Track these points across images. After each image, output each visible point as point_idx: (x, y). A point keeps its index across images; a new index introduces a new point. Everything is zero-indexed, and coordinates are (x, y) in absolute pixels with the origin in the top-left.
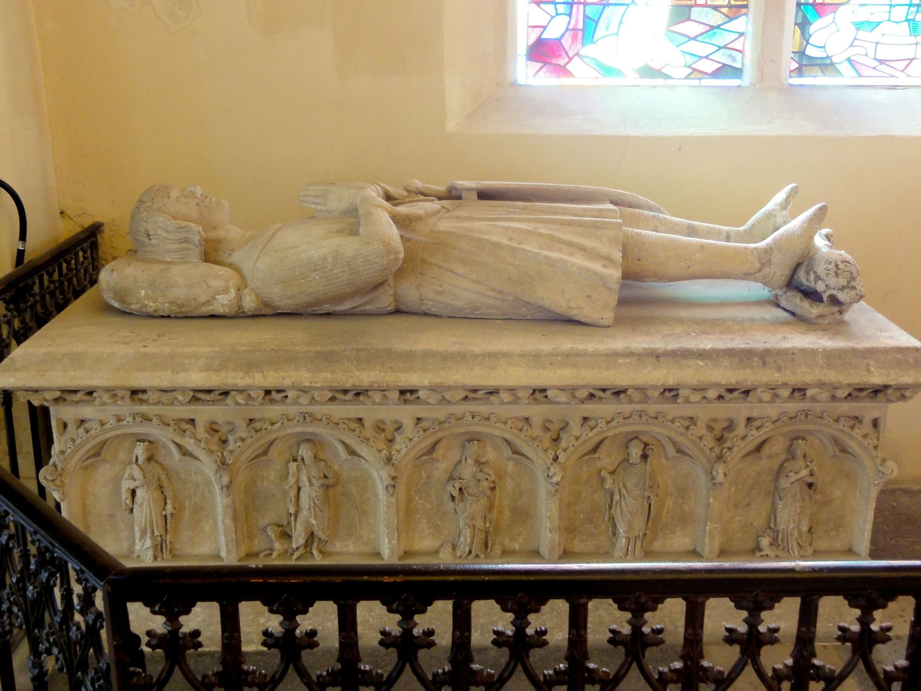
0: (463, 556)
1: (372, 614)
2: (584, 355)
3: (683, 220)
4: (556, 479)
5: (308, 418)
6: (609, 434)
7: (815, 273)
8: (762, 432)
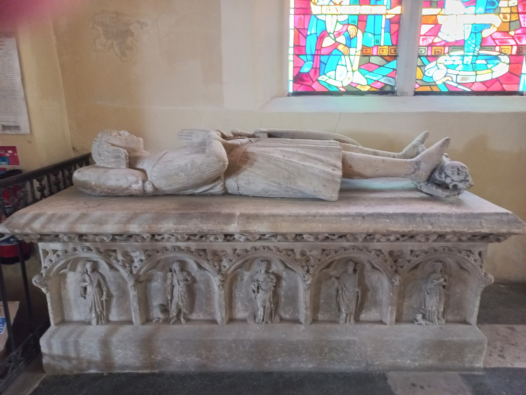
0: (259, 323)
1: (212, 353)
2: (323, 216)
3: (371, 149)
4: (308, 282)
5: (176, 249)
6: (336, 258)
7: (445, 173)
8: (420, 258)
